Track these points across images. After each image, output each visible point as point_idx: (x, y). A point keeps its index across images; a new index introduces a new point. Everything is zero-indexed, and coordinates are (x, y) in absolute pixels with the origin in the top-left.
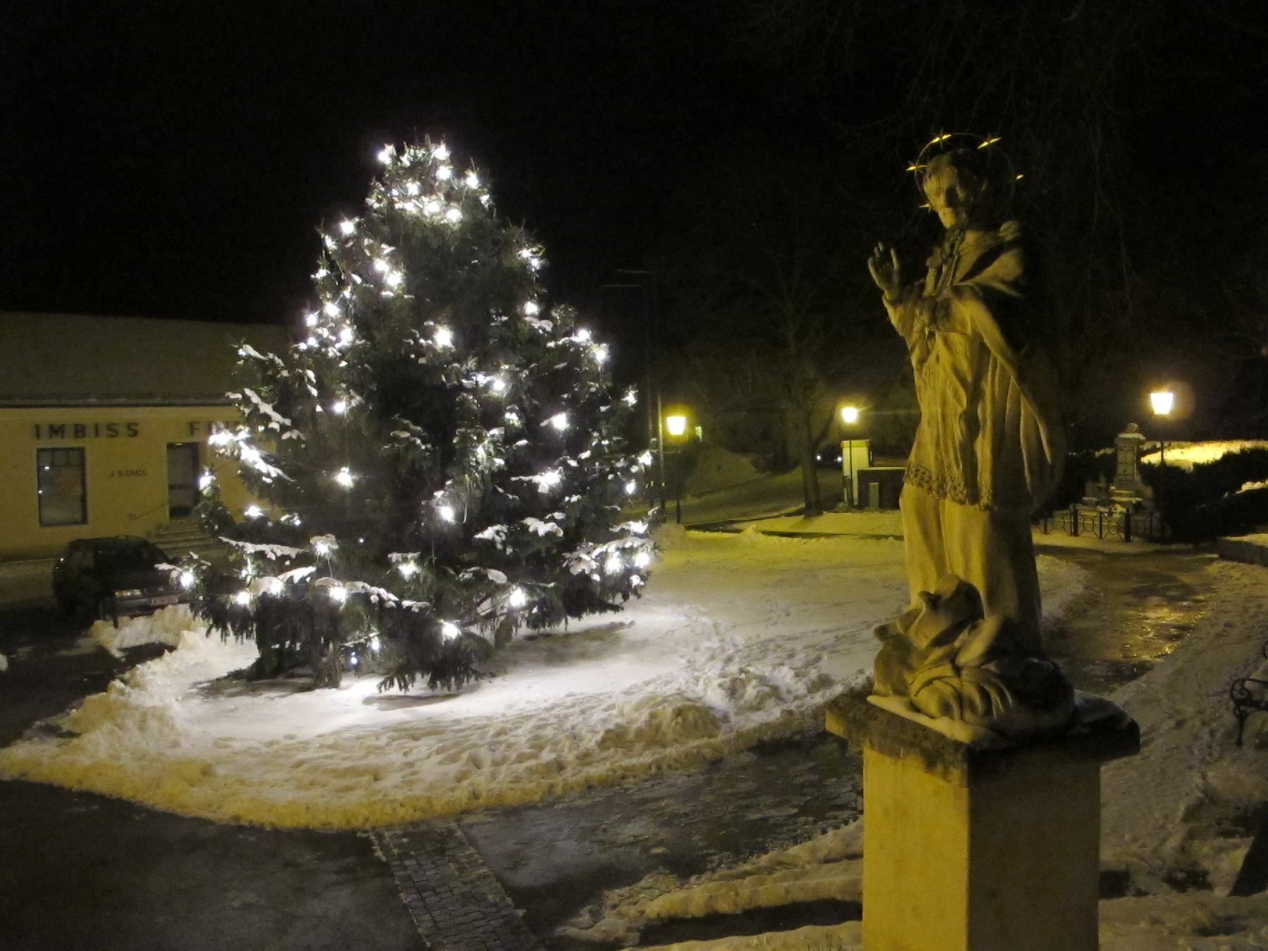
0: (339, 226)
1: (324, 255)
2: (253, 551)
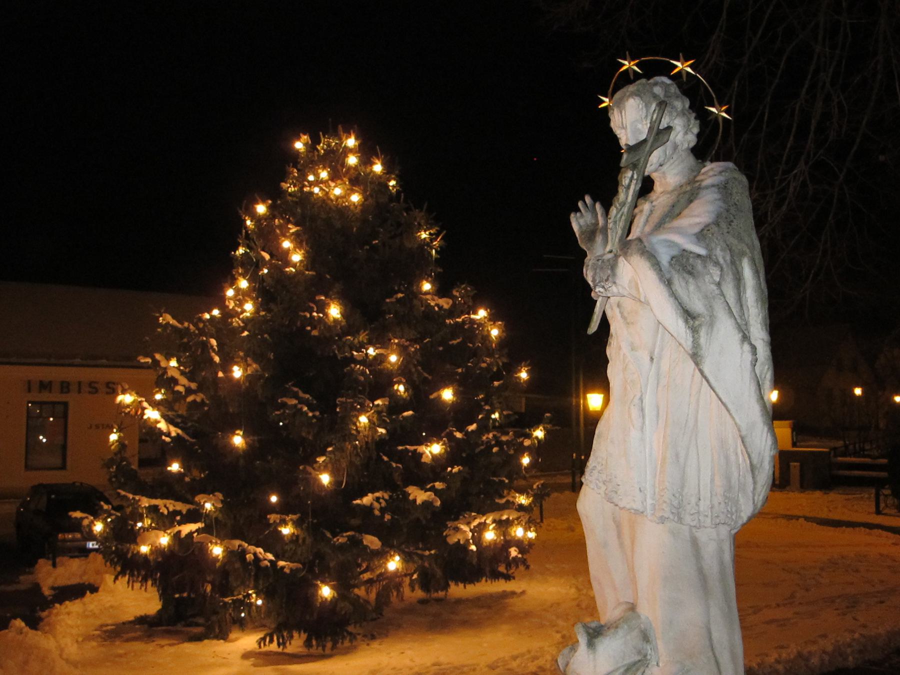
1: (244, 234)
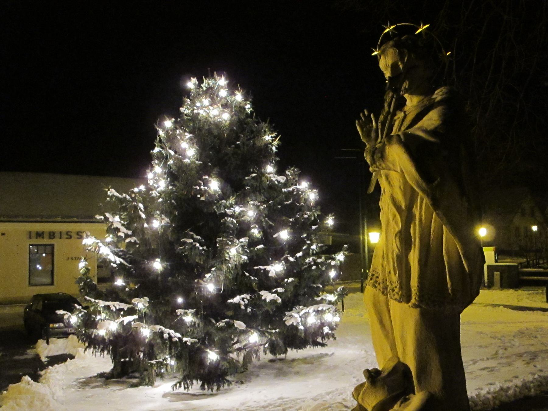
0: (163, 123)
2: (103, 305)
